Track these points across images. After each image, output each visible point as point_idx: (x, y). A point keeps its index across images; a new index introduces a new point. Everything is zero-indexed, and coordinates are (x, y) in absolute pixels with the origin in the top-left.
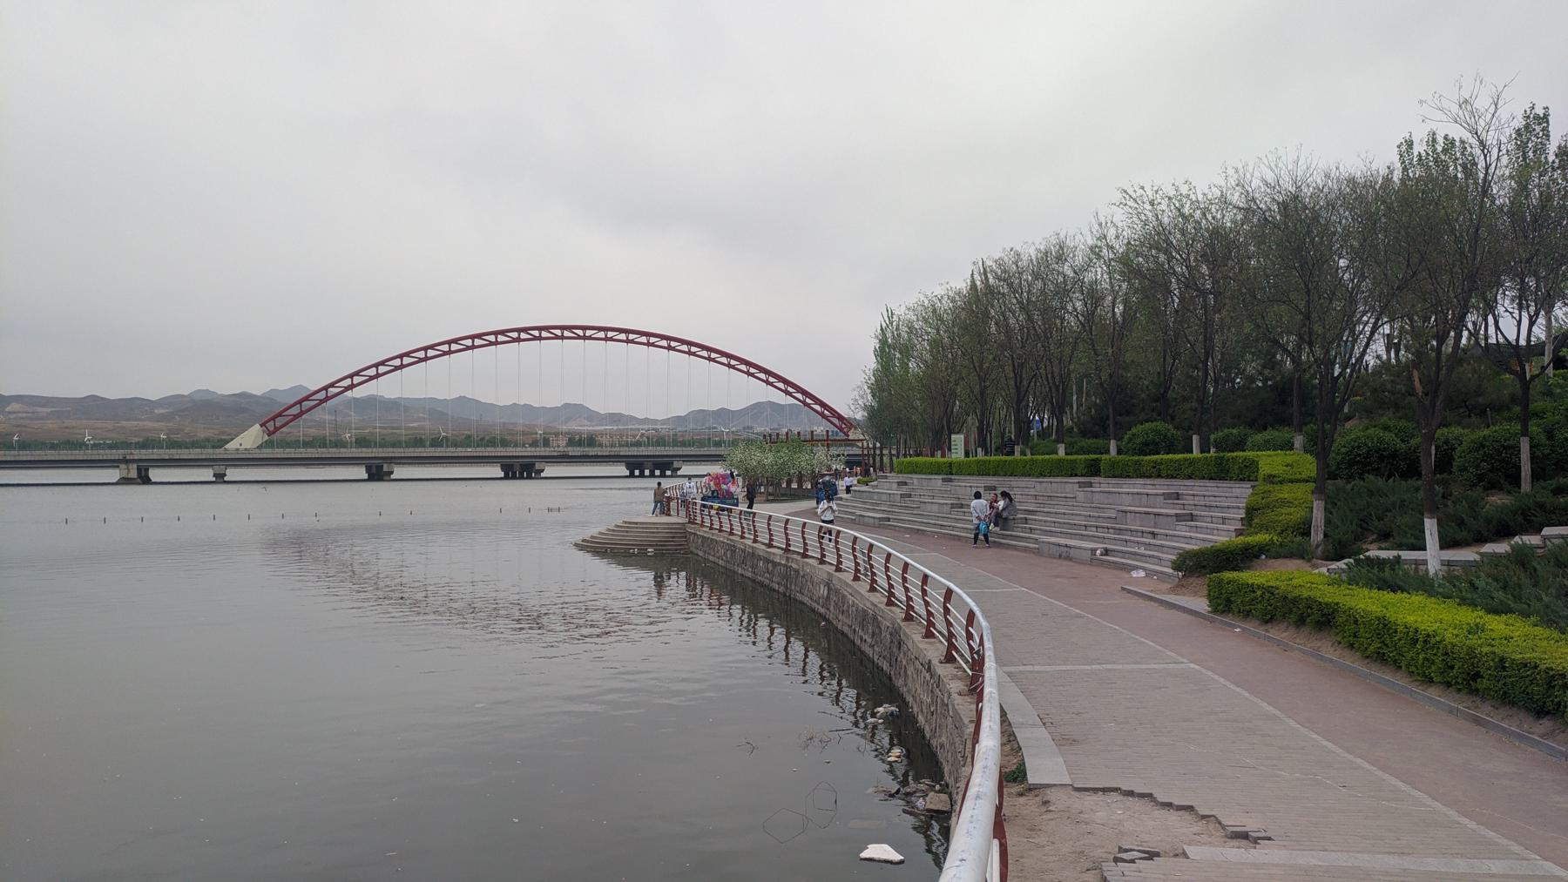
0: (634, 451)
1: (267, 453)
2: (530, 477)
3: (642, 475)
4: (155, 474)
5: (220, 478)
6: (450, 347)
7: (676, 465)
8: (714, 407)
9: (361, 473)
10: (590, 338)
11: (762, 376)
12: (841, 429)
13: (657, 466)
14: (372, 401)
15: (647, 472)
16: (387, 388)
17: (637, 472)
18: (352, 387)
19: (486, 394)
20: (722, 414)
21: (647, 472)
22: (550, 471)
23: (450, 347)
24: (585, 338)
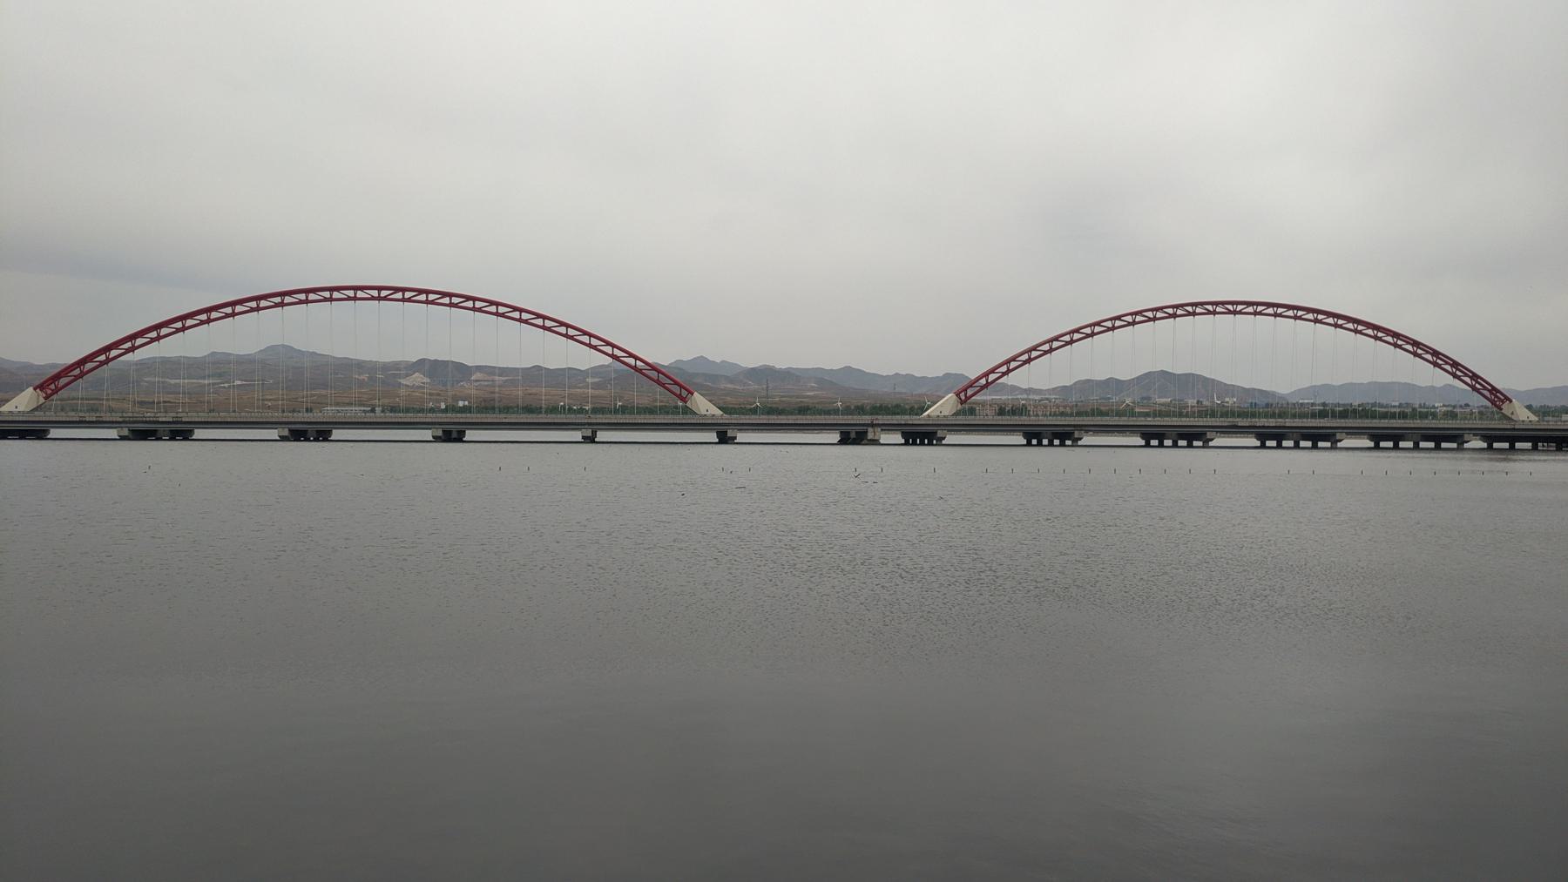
0: (1150, 421)
1: (961, 420)
2: (930, 444)
3: (1040, 444)
4: (602, 436)
5: (590, 440)
6: (1071, 338)
7: (1076, 435)
8: (1179, 370)
9: (835, 437)
10: (1240, 312)
11: (1370, 332)
12: (1493, 403)
13: (1056, 435)
14: (172, 366)
15: (1045, 442)
16: (1020, 378)
17: (1034, 442)
18: (132, 349)
19: (302, 343)
20: (1112, 384)
21: (1045, 442)
22: (950, 439)
23: (1071, 338)
24: (1235, 313)
